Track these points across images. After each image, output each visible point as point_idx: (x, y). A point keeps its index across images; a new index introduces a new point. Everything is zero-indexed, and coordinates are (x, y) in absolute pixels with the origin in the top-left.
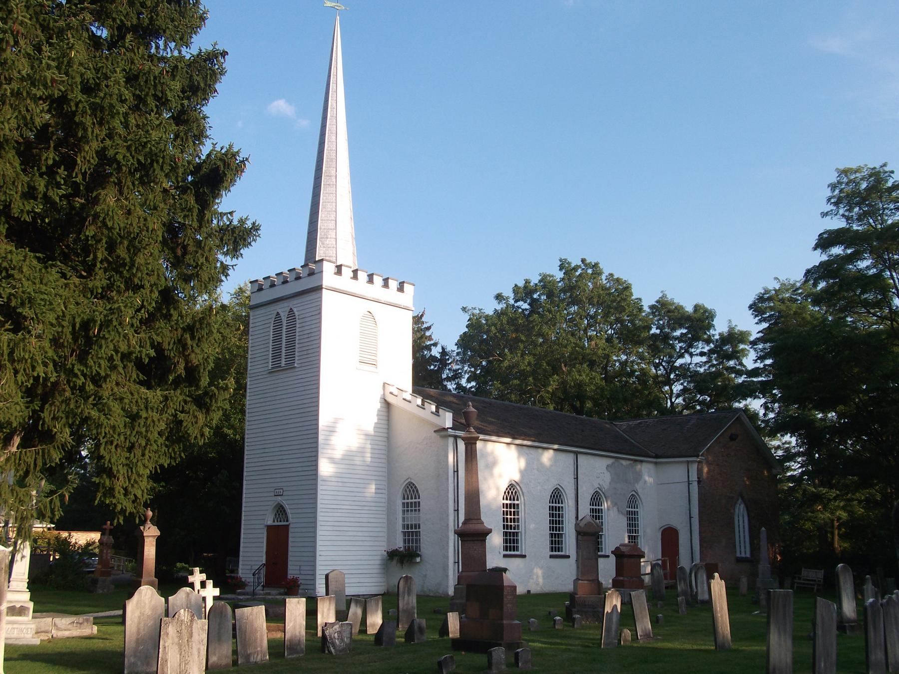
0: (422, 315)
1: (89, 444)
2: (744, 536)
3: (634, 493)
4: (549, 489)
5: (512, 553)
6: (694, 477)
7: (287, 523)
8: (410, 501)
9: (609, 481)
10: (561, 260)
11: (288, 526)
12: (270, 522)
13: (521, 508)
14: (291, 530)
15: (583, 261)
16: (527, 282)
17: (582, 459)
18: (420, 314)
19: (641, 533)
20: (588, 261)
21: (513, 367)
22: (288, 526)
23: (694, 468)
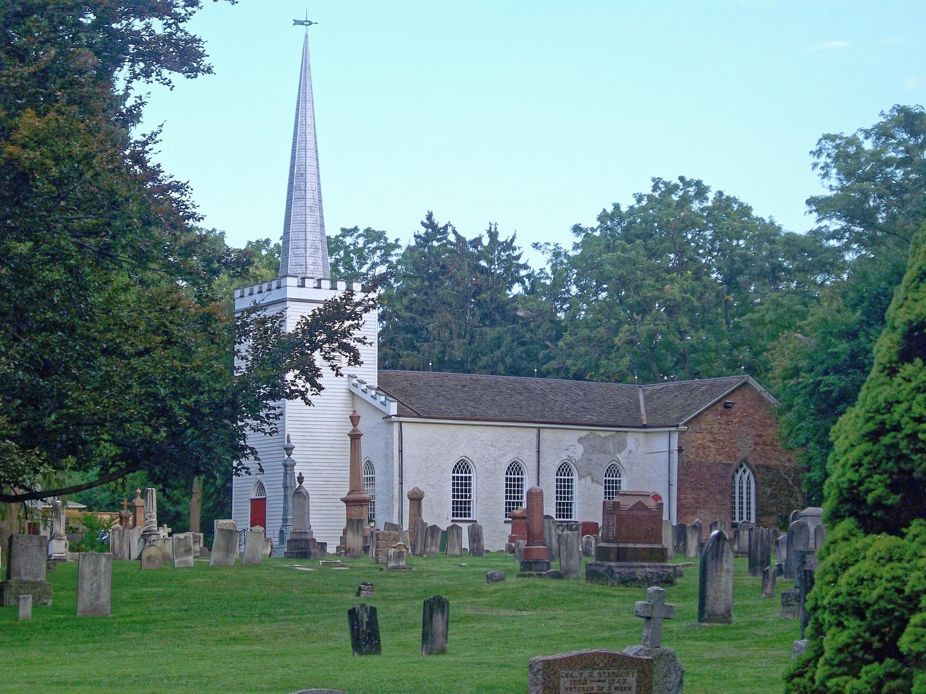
0: (512, 240)
1: (34, 30)
2: (749, 499)
3: (614, 463)
4: (506, 462)
5: (463, 518)
6: (675, 446)
7: (264, 497)
8: (369, 476)
9: (581, 452)
10: (654, 180)
11: (265, 499)
12: (254, 497)
13: (473, 482)
14: (267, 502)
15: (682, 179)
16: (617, 207)
17: (545, 434)
18: (511, 238)
19: (473, 498)
20: (688, 179)
21: (56, 514)
22: (265, 499)
23: (675, 437)
